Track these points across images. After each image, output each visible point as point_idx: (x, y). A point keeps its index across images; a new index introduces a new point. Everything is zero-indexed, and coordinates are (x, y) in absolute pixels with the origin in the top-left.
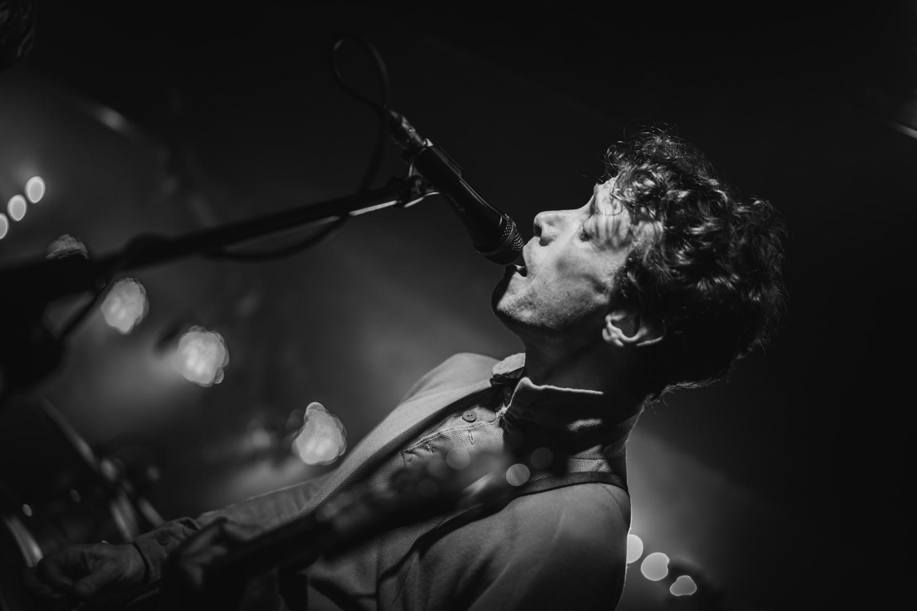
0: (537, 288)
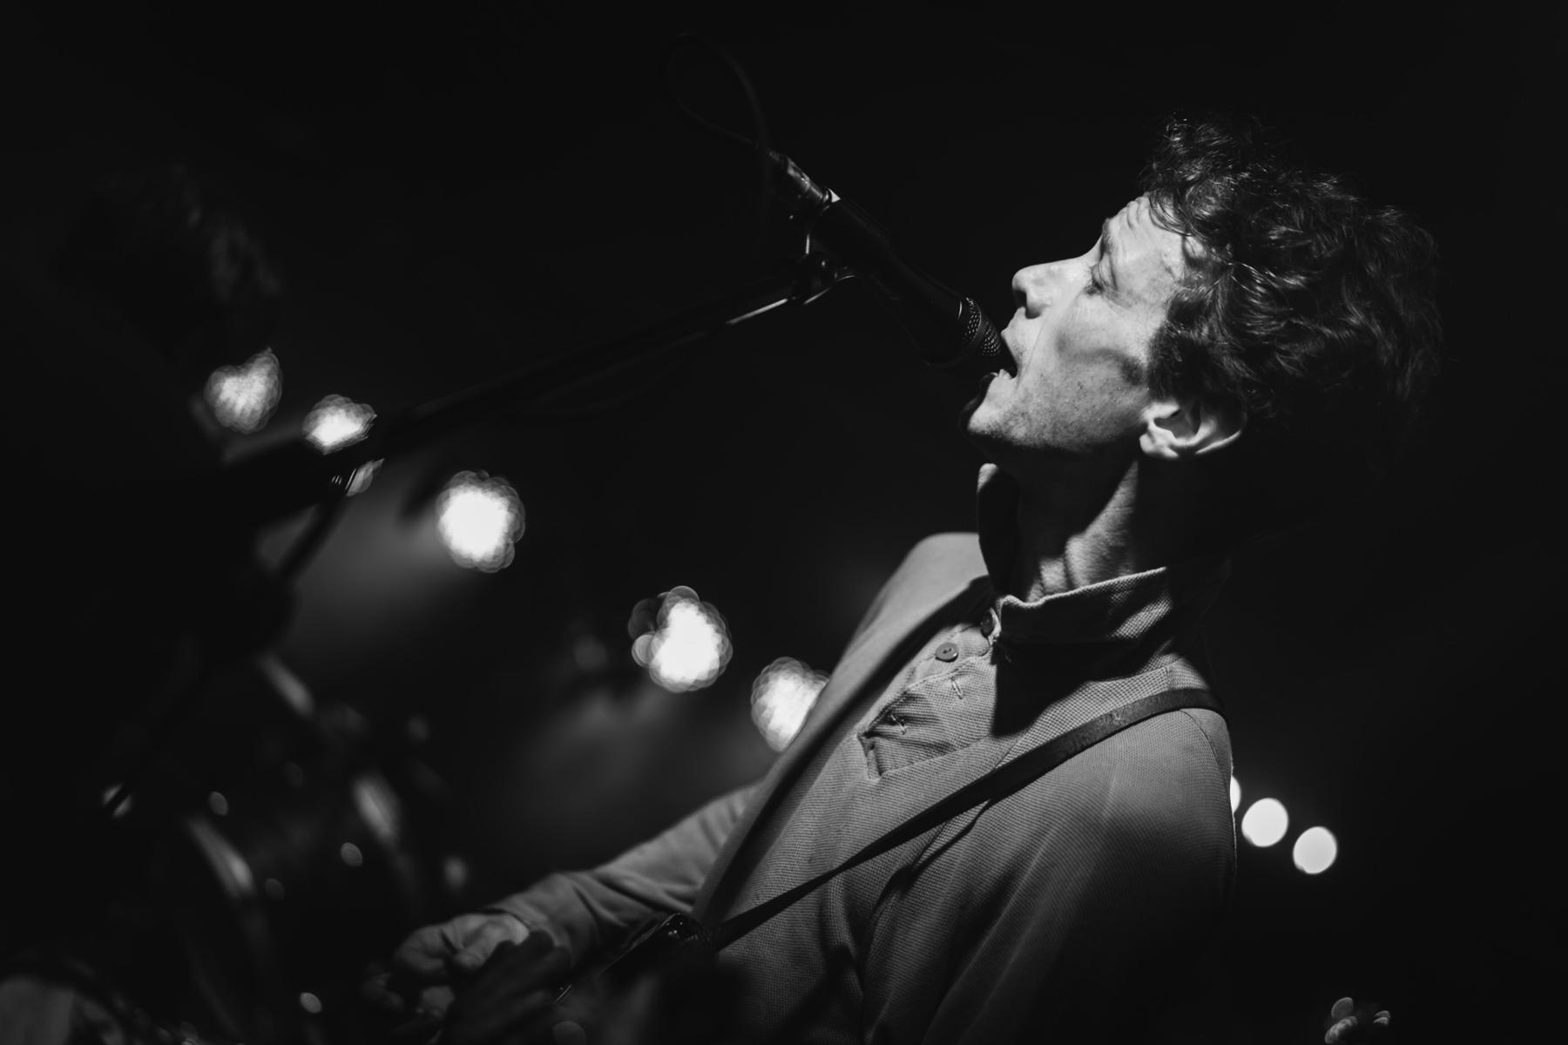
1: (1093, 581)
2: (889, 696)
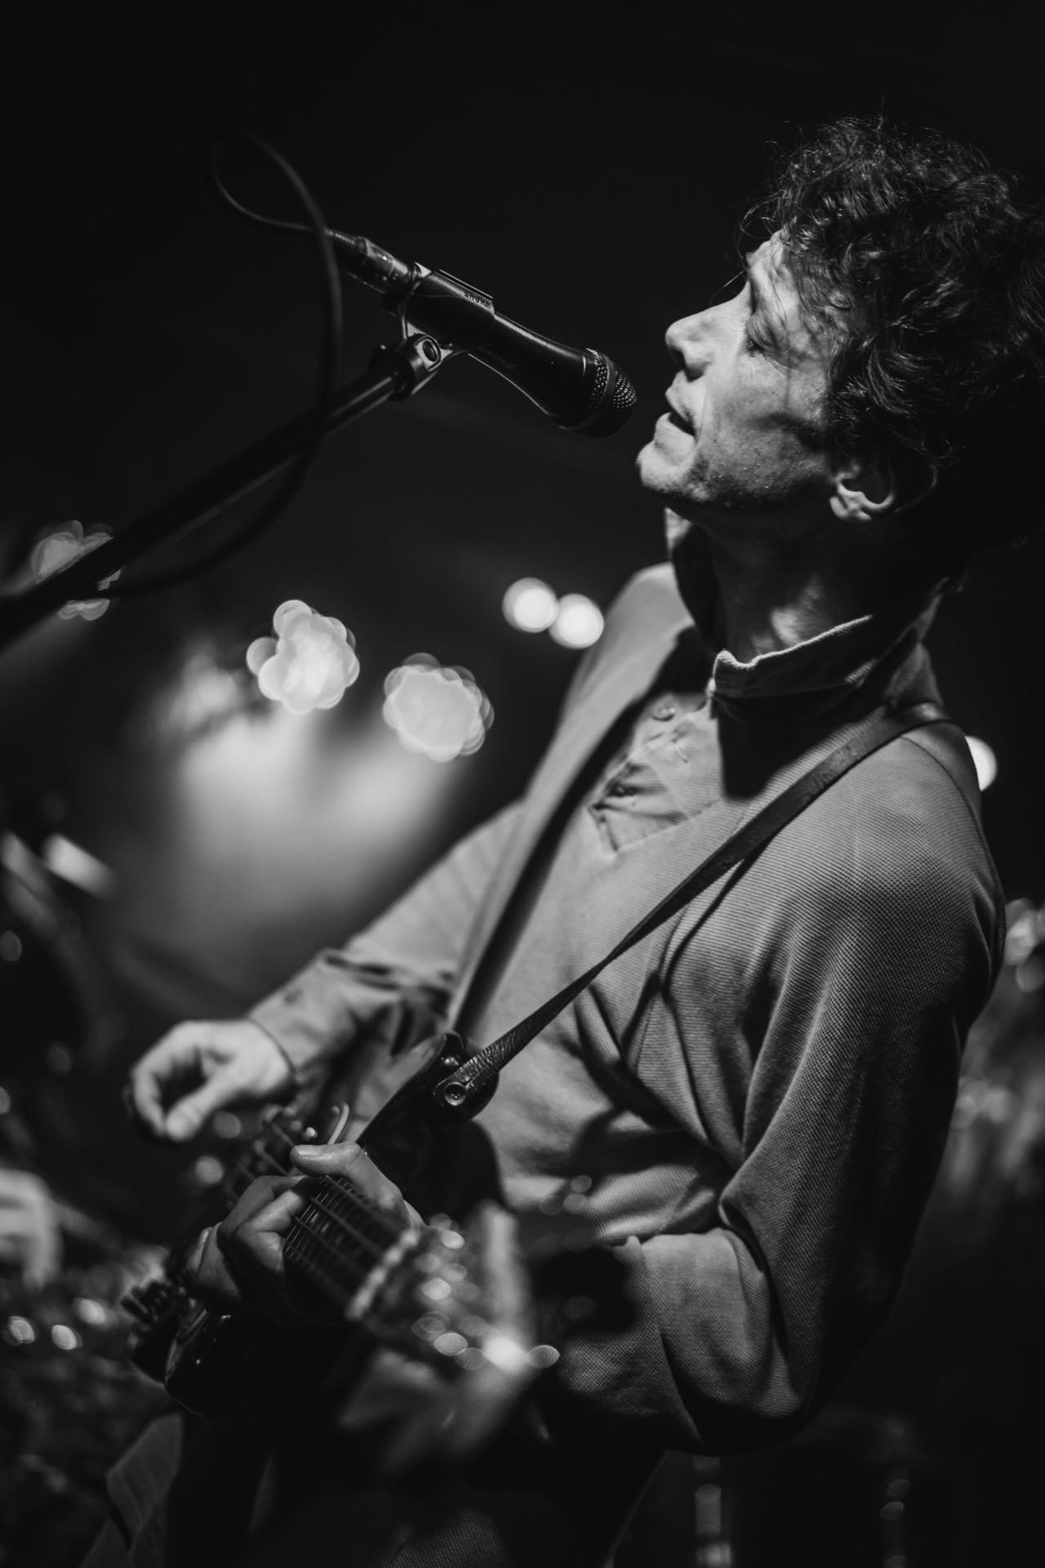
0: (705, 452)
1: (804, 637)
2: (613, 771)
